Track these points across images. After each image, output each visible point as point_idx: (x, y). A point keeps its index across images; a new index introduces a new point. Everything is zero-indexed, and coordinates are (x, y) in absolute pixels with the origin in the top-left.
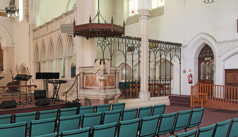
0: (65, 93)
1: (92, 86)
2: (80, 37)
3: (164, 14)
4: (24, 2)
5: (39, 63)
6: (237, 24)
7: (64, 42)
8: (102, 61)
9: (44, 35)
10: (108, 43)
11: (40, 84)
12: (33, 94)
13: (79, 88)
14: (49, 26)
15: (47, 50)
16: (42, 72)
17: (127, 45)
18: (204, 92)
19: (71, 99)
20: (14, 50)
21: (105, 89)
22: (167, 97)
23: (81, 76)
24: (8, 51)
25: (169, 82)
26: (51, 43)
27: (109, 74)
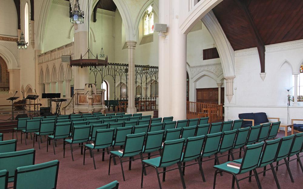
0: (64, 108)
1: (84, 102)
2: (77, 66)
3: (153, 41)
4: (31, 30)
5: (44, 84)
6: (203, 54)
7: (65, 68)
8: (90, 85)
9: (48, 61)
10: (99, 69)
11: (45, 103)
12: (39, 111)
13: (74, 104)
14: (53, 54)
15: (50, 73)
16: (47, 93)
17: (115, 70)
18: (206, 108)
19: (68, 113)
20: (19, 72)
21: (92, 105)
22: (153, 112)
23: (76, 95)
24: (14, 73)
25: (155, 99)
26: (54, 68)
27: (96, 94)
